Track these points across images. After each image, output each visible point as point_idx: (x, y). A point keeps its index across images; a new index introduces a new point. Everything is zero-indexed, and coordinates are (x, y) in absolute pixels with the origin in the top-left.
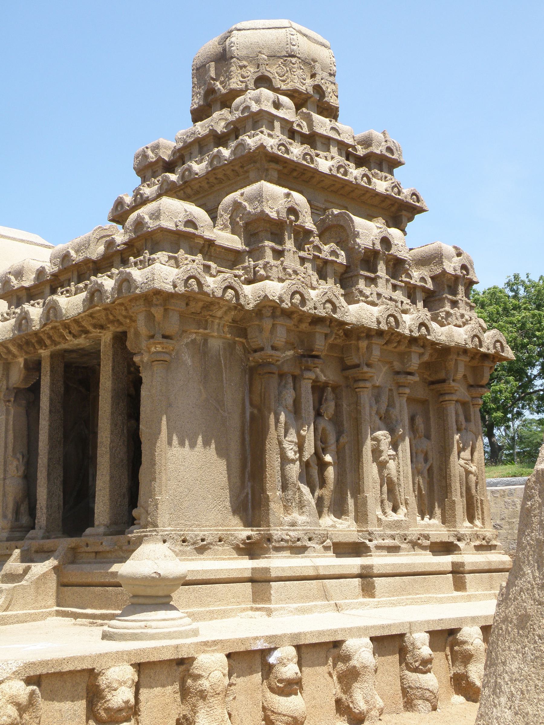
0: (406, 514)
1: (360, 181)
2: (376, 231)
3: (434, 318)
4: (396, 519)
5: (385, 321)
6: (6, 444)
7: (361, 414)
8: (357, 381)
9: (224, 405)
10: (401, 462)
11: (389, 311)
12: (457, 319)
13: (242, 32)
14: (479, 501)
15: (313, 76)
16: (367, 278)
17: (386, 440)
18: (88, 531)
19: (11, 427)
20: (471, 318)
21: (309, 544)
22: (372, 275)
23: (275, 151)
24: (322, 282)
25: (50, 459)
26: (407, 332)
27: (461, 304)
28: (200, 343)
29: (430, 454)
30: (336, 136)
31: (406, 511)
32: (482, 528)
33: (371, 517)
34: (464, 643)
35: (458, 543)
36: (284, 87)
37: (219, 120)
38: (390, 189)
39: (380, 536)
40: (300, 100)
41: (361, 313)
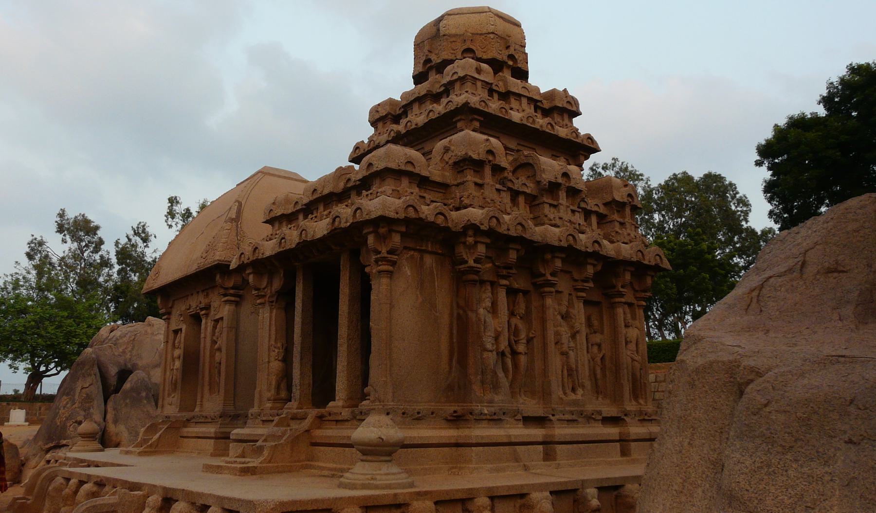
2: (557, 168)
3: (607, 237)
6: (270, 335)
8: (542, 286)
15: (508, 47)
16: (551, 205)
18: (331, 404)
19: (273, 322)
21: (503, 417)
22: (555, 203)
23: (478, 106)
24: (515, 208)
25: (302, 348)
26: (583, 249)
27: (628, 225)
29: (603, 346)
30: (526, 94)
34: (627, 496)
36: (485, 57)
37: (435, 82)
39: (561, 411)
40: (497, 65)
41: (551, 233)
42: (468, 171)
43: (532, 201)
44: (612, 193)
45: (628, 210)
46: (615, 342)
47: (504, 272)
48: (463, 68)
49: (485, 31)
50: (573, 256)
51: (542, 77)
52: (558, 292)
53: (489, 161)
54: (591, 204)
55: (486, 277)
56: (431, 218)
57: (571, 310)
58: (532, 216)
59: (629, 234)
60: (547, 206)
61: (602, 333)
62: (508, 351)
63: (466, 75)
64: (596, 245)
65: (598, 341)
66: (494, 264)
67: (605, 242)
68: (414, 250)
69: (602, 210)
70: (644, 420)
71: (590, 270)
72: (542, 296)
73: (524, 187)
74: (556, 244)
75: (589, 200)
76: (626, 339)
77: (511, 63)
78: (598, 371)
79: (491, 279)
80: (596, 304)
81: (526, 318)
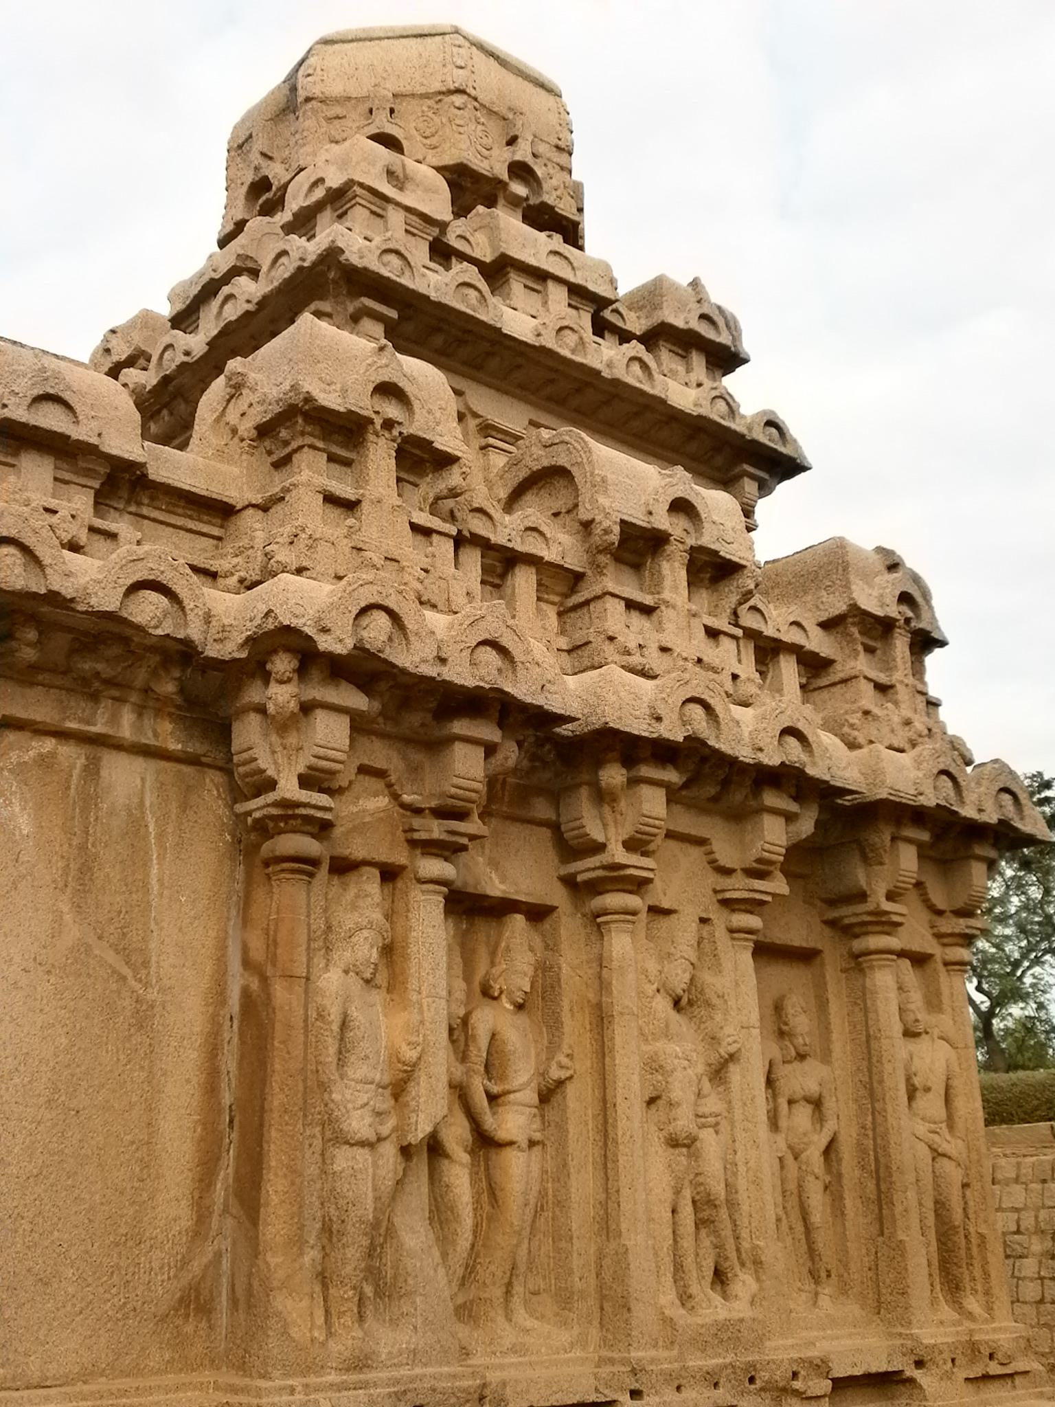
0: (754, 1297)
1: (624, 372)
4: (722, 1314)
5: (675, 716)
7: (611, 993)
8: (595, 888)
9: (146, 964)
10: (740, 1135)
11: (688, 687)
12: (892, 731)
13: (336, 46)
14: (974, 1240)
15: (512, 141)
16: (631, 605)
17: (689, 1071)
20: (930, 730)
22: (648, 600)
26: (745, 754)
27: (902, 693)
28: (72, 767)
29: (830, 1105)
31: (754, 1286)
32: (986, 1321)
33: (643, 1316)
35: (917, 1374)
38: (706, 403)
39: (668, 1377)
42: (307, 454)
43: (564, 585)
44: (847, 586)
45: (901, 644)
46: (870, 1091)
47: (436, 829)
48: (344, 163)
49: (437, 86)
50: (711, 778)
51: (625, 248)
52: (655, 910)
53: (389, 424)
54: (777, 621)
55: (357, 849)
56: (108, 601)
57: (707, 977)
58: (563, 643)
59: (908, 723)
60: (615, 608)
61: (826, 1057)
62: (457, 1135)
63: (350, 183)
64: (792, 741)
65: (813, 1088)
66: (395, 797)
67: (827, 740)
68: (62, 735)
69: (817, 642)
70: (986, 1377)
71: (773, 835)
72: (597, 923)
73: (532, 538)
74: (641, 728)
75: (771, 611)
76: (908, 1080)
77: (519, 189)
78: (817, 1199)
79: (383, 856)
80: (805, 956)
81: (539, 1002)
